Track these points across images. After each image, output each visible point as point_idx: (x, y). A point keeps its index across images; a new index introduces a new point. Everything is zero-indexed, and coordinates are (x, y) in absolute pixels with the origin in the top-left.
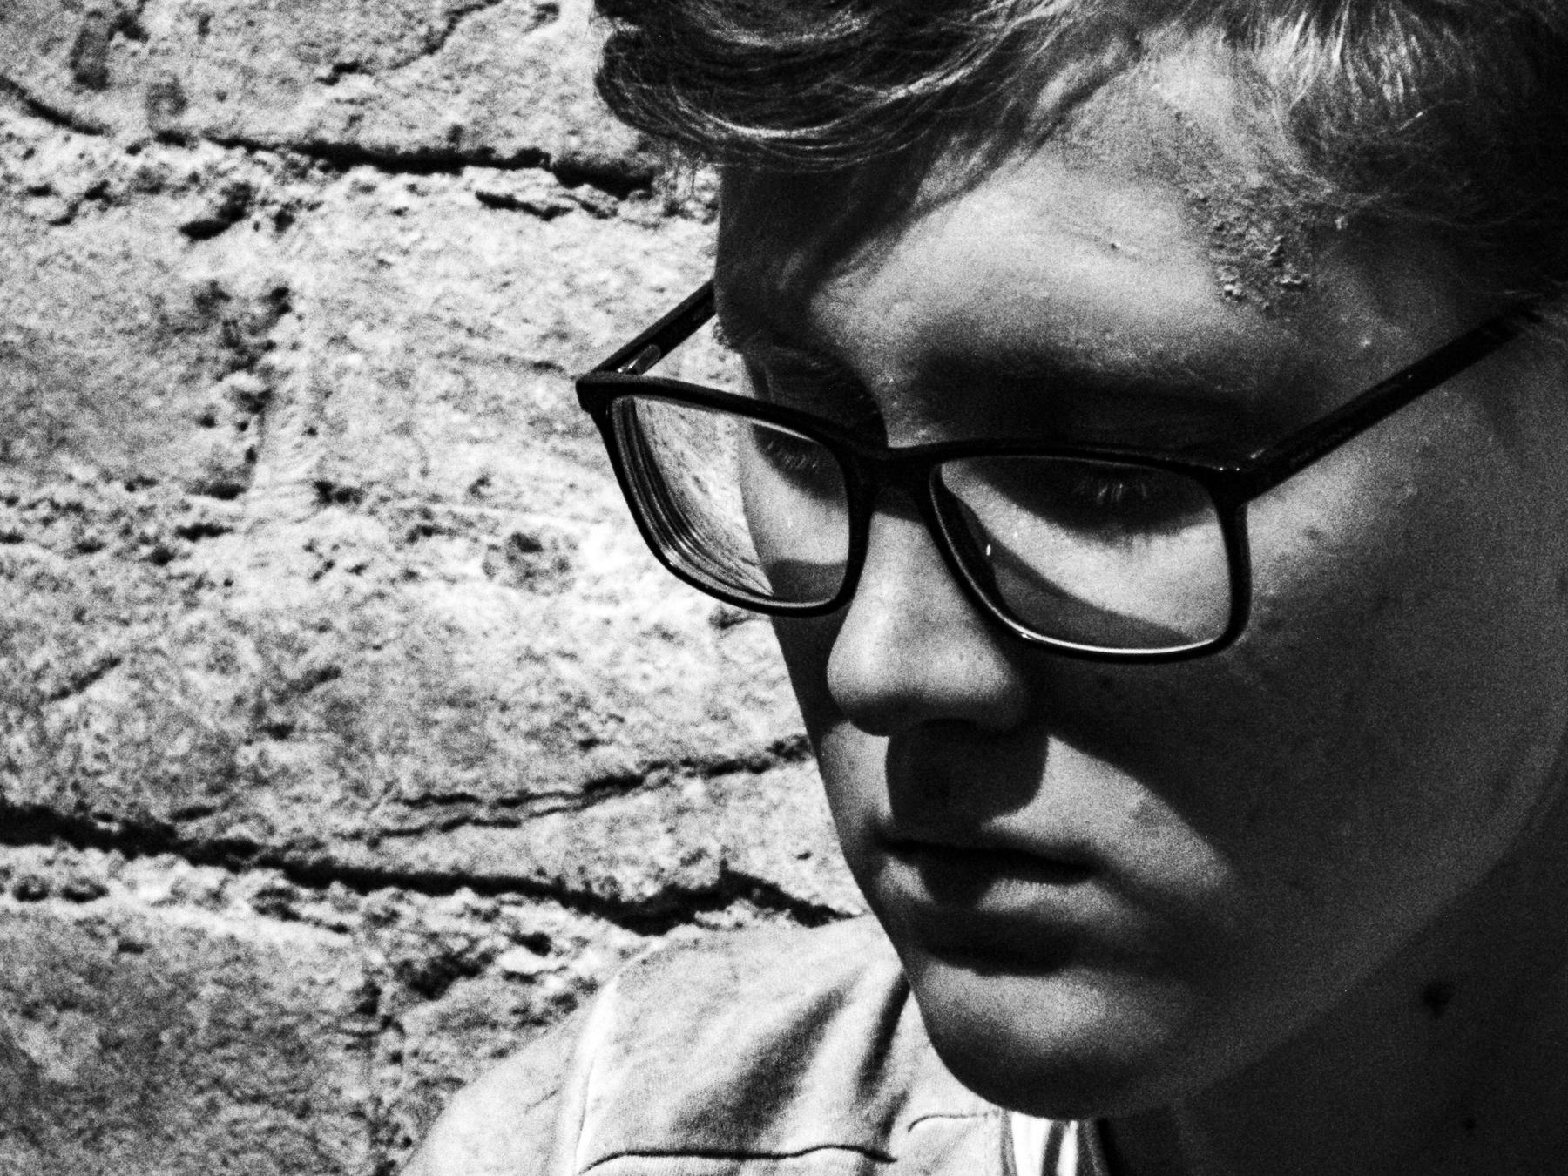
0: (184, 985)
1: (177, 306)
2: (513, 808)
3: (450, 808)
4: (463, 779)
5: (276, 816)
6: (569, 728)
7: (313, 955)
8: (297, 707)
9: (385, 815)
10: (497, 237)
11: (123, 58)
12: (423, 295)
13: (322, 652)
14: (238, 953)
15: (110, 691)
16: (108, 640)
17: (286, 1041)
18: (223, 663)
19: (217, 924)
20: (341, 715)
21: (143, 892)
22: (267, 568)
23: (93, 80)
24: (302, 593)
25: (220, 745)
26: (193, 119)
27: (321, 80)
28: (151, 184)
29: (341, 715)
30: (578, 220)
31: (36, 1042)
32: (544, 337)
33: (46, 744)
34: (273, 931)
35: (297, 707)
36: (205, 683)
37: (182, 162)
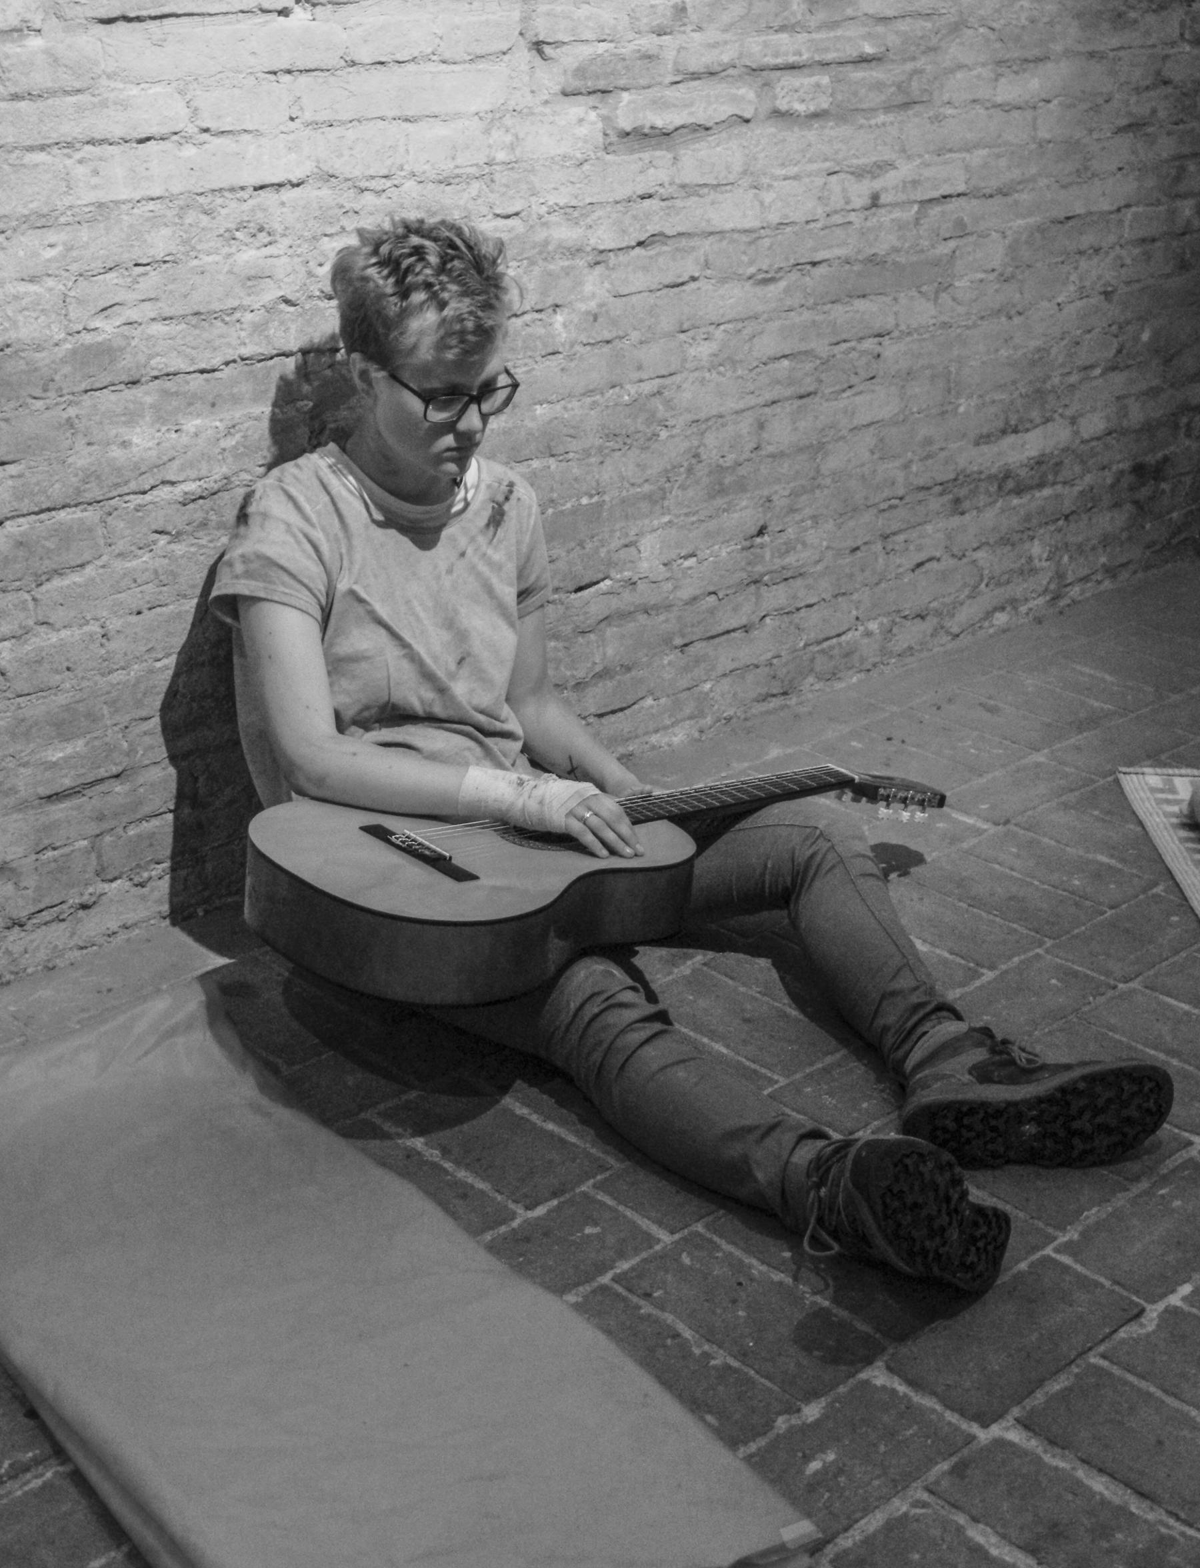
0: (71, 527)
1: (63, 421)
2: (126, 483)
3: (117, 485)
4: (119, 480)
5: (88, 496)
6: (136, 466)
7: (91, 515)
8: (409, 360)
9: (106, 490)
10: (113, 397)
11: (51, 385)
12: (103, 409)
13: (93, 469)
14: (80, 519)
15: (57, 486)
16: (57, 477)
17: (90, 530)
18: (76, 475)
19: (75, 516)
20: (98, 477)
21: (62, 515)
22: (82, 458)
23: (45, 390)
24: (89, 460)
25: (78, 488)
26: (65, 392)
27: (383, 242)
28: (57, 404)
29: (98, 477)
30: (127, 391)
31: (47, 544)
32: (500, 251)
33: (48, 497)
34: (85, 514)
35: (409, 360)
36: (74, 479)
37: (63, 399)
